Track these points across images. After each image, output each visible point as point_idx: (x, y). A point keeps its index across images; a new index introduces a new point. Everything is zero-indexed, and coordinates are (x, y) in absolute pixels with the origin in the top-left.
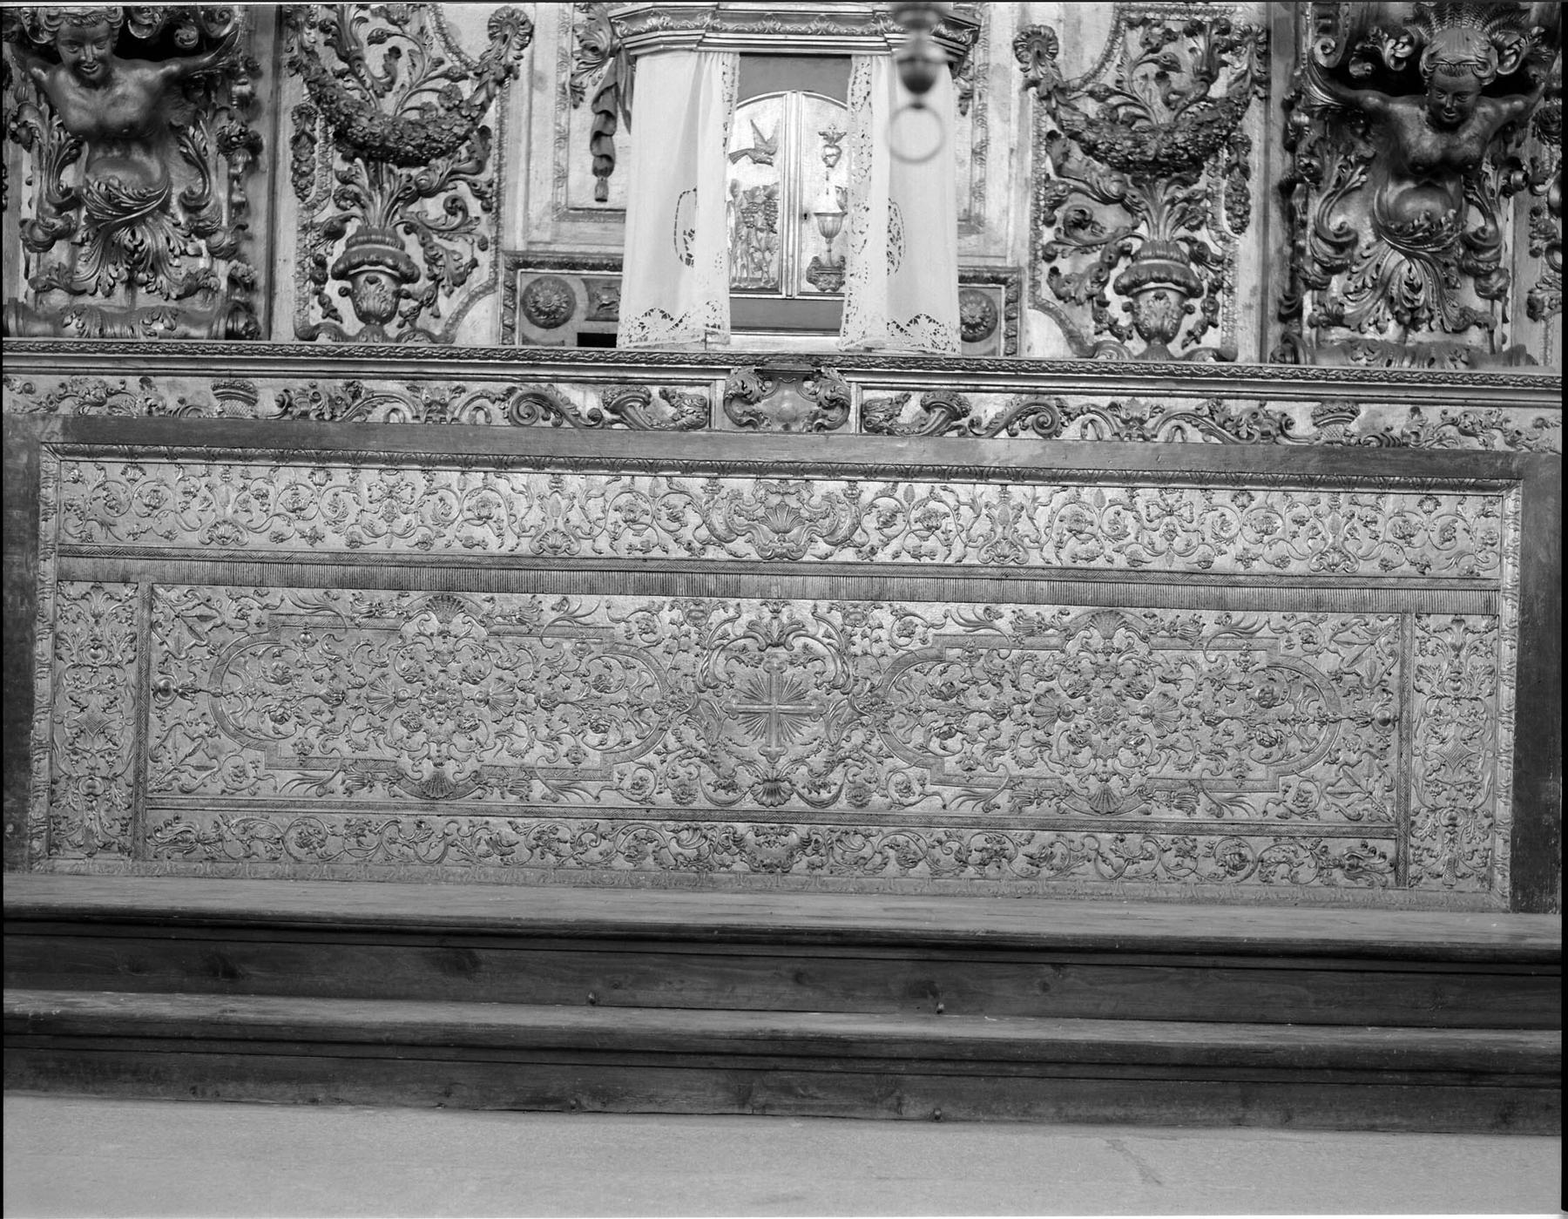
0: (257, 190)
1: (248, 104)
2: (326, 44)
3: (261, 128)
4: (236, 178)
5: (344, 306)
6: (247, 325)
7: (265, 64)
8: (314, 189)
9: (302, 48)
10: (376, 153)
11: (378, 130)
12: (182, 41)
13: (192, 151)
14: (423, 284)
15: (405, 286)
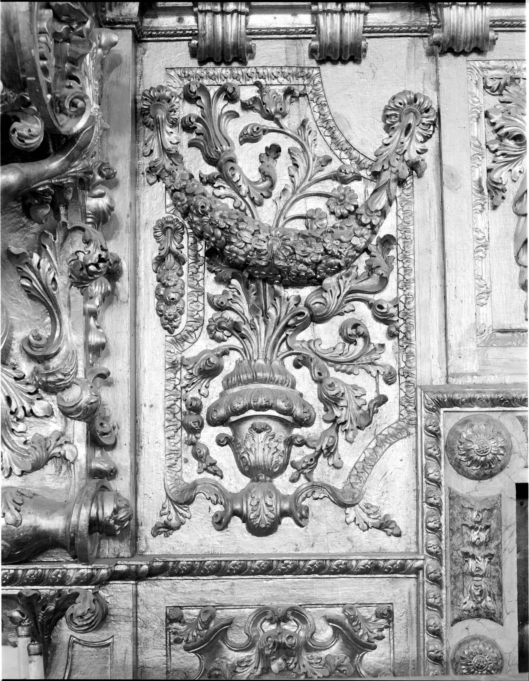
0: (114, 325)
1: (105, 221)
2: (190, 145)
3: (119, 248)
4: (94, 314)
5: (224, 457)
6: (115, 511)
7: (122, 170)
8: (184, 318)
9: (164, 150)
10: (258, 274)
11: (265, 246)
12: (21, 138)
13: (37, 285)
14: (319, 427)
15: (296, 431)
